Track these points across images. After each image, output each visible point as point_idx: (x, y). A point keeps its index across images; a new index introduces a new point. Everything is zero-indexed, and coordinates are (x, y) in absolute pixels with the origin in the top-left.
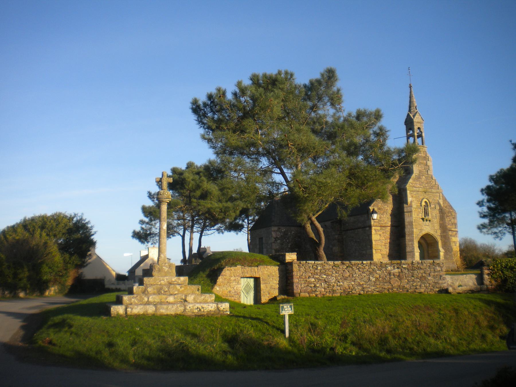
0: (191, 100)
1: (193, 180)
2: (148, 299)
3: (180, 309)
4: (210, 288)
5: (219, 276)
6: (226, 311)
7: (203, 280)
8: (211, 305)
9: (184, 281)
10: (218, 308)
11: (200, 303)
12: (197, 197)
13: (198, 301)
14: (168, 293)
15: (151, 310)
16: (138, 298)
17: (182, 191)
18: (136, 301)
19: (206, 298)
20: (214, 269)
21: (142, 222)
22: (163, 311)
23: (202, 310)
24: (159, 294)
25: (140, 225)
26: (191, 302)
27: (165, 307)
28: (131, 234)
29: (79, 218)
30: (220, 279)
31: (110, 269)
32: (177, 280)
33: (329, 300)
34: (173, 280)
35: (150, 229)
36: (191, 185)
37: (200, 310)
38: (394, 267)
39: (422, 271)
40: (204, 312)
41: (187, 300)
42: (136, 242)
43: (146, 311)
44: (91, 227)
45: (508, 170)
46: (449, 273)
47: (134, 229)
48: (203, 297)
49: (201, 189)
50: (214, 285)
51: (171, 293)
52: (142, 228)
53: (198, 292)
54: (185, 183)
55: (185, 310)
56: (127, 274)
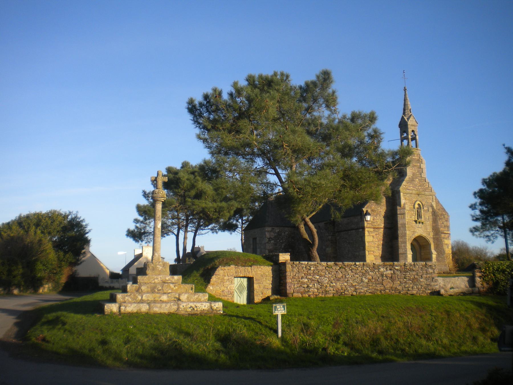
1: (187, 179)
2: (142, 297)
5: (213, 275)
8: (204, 304)
9: (178, 280)
10: (211, 307)
11: (194, 302)
13: (192, 300)
15: (144, 308)
18: (130, 300)
19: (200, 297)
21: (136, 221)
22: (157, 309)
23: (196, 309)
24: (153, 293)
25: (134, 224)
26: (184, 301)
27: (159, 305)
28: (126, 233)
29: (73, 216)
30: (214, 279)
31: (104, 267)
34: (167, 278)
36: (185, 185)
37: (193, 309)
38: (387, 268)
40: (197, 311)
41: (181, 298)
42: (130, 240)
43: (140, 310)
48: (196, 296)
49: (196, 188)
51: (165, 292)
52: (137, 227)
53: (191, 291)
56: (121, 273)
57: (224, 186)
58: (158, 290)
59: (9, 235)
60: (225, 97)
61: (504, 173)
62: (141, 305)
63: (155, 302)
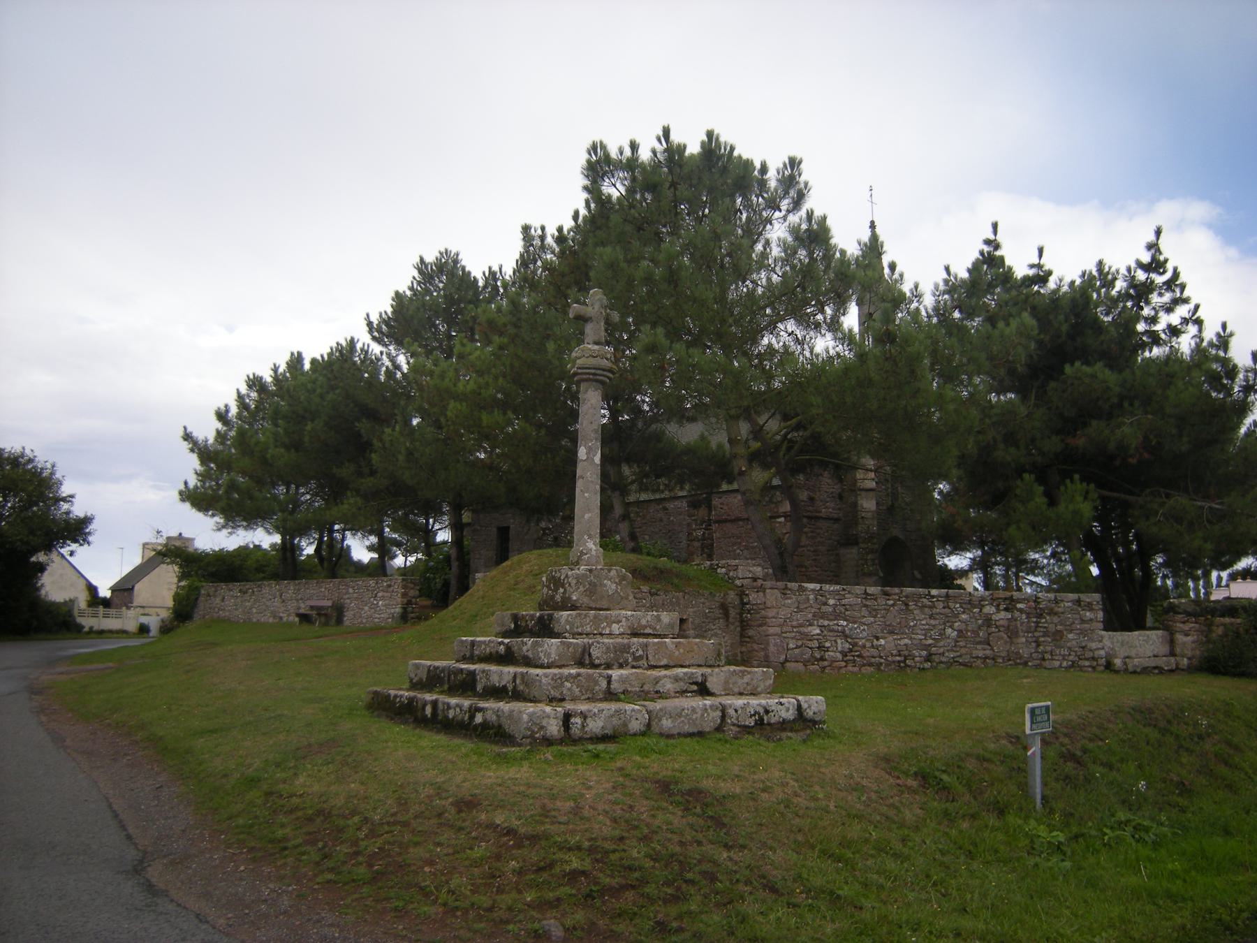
13: (736, 690)
38: (998, 606)
39: (1056, 619)
45: (54, 604)
46: (288, 554)
58: (636, 659)
61: (351, 558)
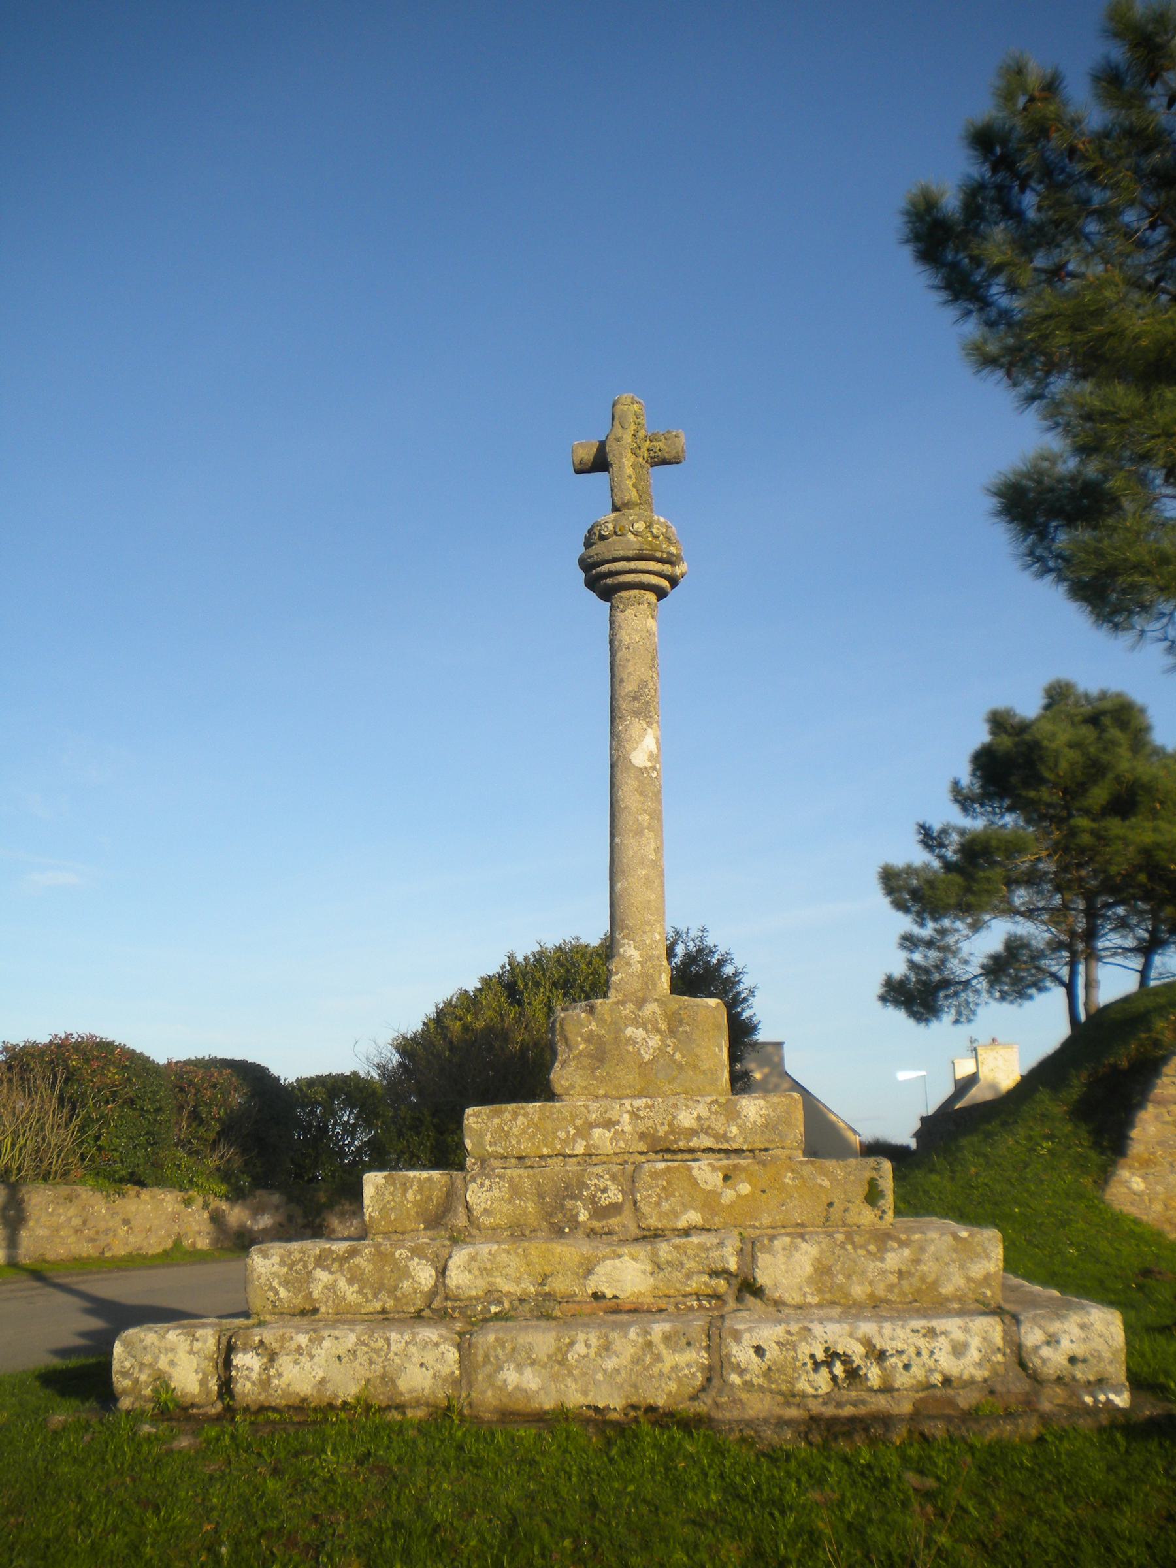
0: (901, 201)
1: (1071, 745)
2: (442, 1272)
3: (668, 1370)
4: (1087, 1181)
5: (1141, 1105)
6: (1101, 1383)
7: (1050, 1137)
8: (952, 1326)
9: (770, 1126)
10: (1020, 1358)
11: (876, 1307)
12: (1096, 808)
13: (858, 1291)
14: (624, 1221)
15: (422, 1365)
16: (362, 1262)
17: (1032, 794)
18: (350, 1292)
19: (928, 1267)
20: (1114, 1068)
21: (909, 942)
22: (526, 1377)
23: (874, 1374)
24: (559, 1232)
25: (904, 955)
26: (792, 1297)
27: (542, 1340)
28: (879, 990)
29: (692, 947)
30: (1148, 1128)
31: (841, 1124)
32: (719, 1125)
33: (565, 1061)
34: (686, 1119)
35: (940, 966)
36: (1063, 765)
37: (853, 1374)
40: (887, 1389)
41: (763, 1278)
42: (898, 1017)
43: (387, 1379)
44: (736, 974)
47: (888, 970)
48: (894, 1259)
49: (1110, 776)
50: (1114, 1163)
51: (653, 1222)
52: (913, 965)
53: (867, 1216)
54: (1041, 758)
55: (714, 1373)
56: (913, 1144)
57: (1140, 552)
58: (600, 1212)
59: (466, 1028)
60: (1088, 110)
62: (397, 1339)
63: (545, 1308)
